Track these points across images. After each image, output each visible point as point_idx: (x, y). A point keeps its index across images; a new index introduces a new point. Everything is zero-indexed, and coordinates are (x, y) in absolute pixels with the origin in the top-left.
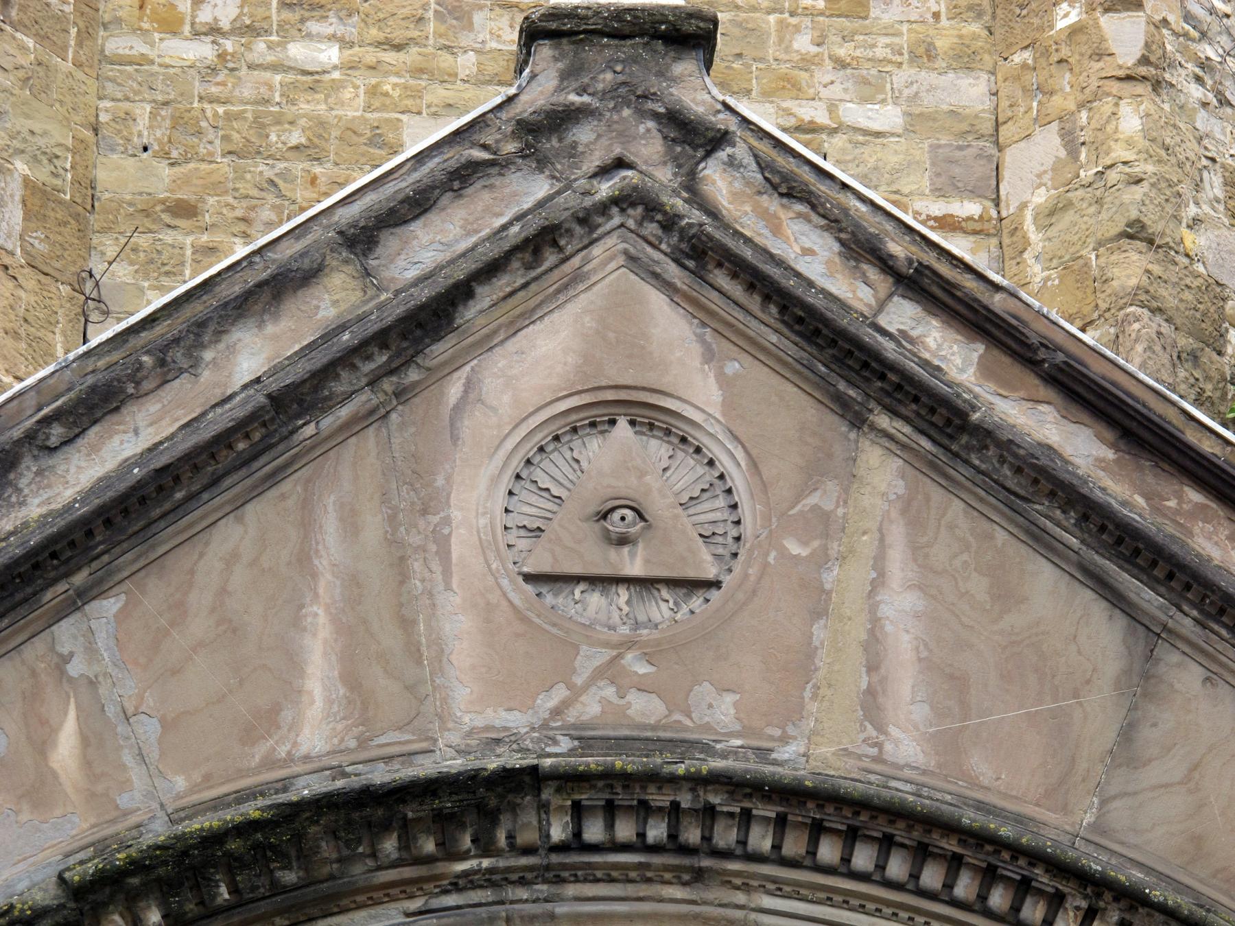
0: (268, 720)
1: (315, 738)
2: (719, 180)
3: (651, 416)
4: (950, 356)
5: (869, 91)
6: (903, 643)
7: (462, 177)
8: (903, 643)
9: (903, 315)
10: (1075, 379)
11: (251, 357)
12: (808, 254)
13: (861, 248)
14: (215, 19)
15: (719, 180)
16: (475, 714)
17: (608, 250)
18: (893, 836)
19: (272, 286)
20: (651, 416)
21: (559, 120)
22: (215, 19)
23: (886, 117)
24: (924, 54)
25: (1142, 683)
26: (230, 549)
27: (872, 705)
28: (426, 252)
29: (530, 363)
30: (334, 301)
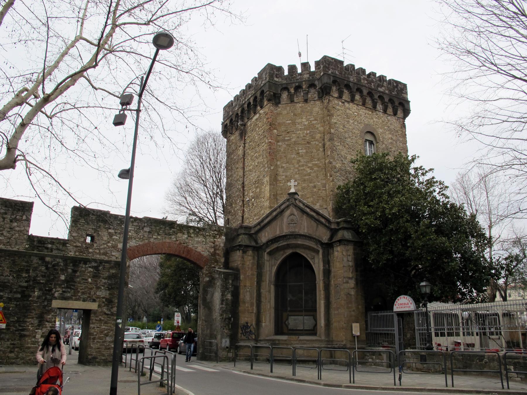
1: (278, 233)
2: (297, 202)
3: (294, 215)
4: (308, 210)
5: (319, 182)
9: (306, 208)
11: (274, 214)
13: (304, 204)
16: (286, 231)
17: (291, 207)
19: (275, 210)
20: (294, 215)
21: (289, 199)
23: (319, 184)
26: (274, 224)
27: (304, 229)
28: (283, 207)
29: (288, 213)
30: (278, 210)
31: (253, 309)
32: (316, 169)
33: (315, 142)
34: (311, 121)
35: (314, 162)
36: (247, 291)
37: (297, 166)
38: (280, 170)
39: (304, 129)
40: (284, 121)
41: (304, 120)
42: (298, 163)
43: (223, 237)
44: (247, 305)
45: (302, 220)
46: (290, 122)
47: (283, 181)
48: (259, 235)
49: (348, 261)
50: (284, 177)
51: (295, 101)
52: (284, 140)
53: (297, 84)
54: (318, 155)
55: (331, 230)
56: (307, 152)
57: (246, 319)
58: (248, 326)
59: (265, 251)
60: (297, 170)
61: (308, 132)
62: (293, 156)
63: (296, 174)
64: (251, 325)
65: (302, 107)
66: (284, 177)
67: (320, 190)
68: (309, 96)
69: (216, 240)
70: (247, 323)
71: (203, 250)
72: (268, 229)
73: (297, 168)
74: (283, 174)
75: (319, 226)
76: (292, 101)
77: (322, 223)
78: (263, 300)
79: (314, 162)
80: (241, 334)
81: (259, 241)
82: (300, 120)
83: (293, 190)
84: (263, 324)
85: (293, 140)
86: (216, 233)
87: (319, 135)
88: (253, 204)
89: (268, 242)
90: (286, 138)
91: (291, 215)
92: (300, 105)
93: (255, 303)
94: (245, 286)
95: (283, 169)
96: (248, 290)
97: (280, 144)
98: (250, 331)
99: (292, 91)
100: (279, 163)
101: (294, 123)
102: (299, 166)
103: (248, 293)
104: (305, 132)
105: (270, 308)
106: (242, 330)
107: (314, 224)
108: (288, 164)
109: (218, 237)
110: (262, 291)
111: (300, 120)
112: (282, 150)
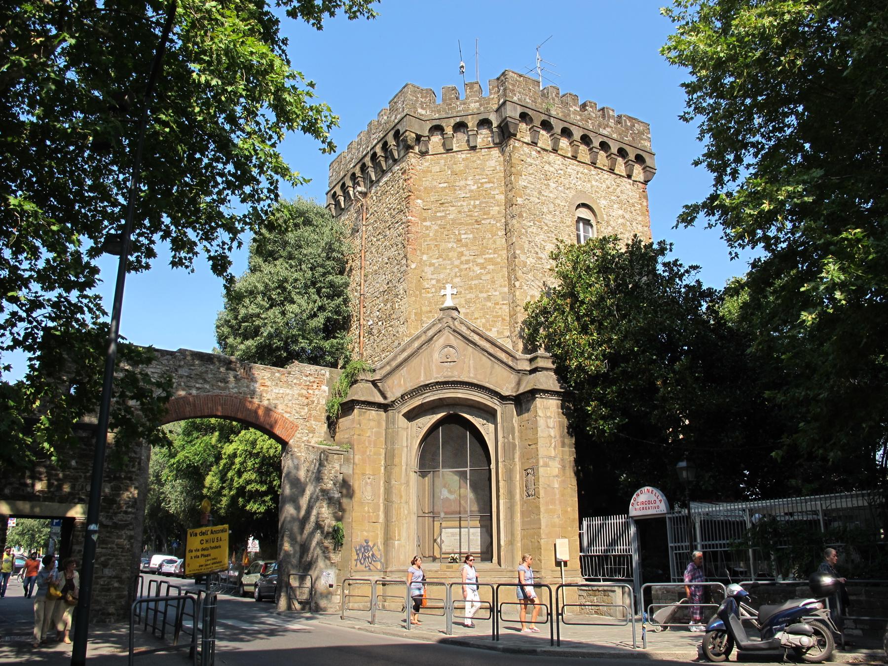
0: (418, 378)
1: (423, 380)
2: (456, 323)
3: (451, 346)
4: (476, 338)
5: (496, 291)
6: (472, 365)
7: (434, 325)
8: (472, 365)
9: (472, 334)
10: (576, 647)
11: (416, 344)
12: (464, 330)
13: (469, 328)
14: (698, 281)
15: (456, 323)
17: (446, 332)
18: (481, 269)
19: (418, 338)
21: (442, 318)
22: (698, 281)
23: (497, 293)
24: (501, 286)
25: (493, 367)
26: (415, 362)
27: (469, 372)
28: (430, 333)
29: (440, 341)
30: (423, 338)
31: (378, 515)
32: (491, 267)
33: (488, 221)
34: (482, 183)
35: (487, 256)
36: (367, 483)
37: (457, 262)
38: (428, 270)
39: (470, 198)
40: (435, 183)
41: (469, 182)
42: (459, 258)
43: (325, 388)
44: (366, 509)
45: (465, 355)
46: (445, 185)
47: (433, 290)
48: (390, 381)
49: (549, 427)
50: (434, 282)
51: (455, 149)
52: (434, 218)
53: (458, 120)
54: (495, 242)
55: (518, 371)
56: (475, 238)
57: (365, 533)
58: (368, 546)
59: (399, 412)
60: (457, 270)
61: (477, 202)
62: (450, 245)
63: (456, 276)
64: (374, 545)
65: (467, 159)
66: (434, 282)
67: (497, 304)
68: (479, 140)
69: (311, 392)
70: (367, 541)
71: (289, 410)
72: (404, 371)
73: (457, 267)
74: (433, 277)
75: (496, 366)
76: (449, 150)
77: (502, 362)
78: (395, 498)
79: (487, 256)
80: (356, 560)
81: (388, 395)
82: (462, 183)
83: (449, 303)
84: (396, 542)
85: (451, 217)
86: (311, 379)
87: (497, 208)
88: (379, 332)
89: (402, 396)
90: (439, 214)
91: (446, 346)
92: (463, 156)
93: (382, 505)
94: (364, 474)
95: (432, 268)
96: (369, 481)
97: (428, 223)
98: (373, 555)
99: (449, 131)
100: (425, 257)
101: (452, 188)
102: (462, 263)
103: (369, 488)
104: (472, 203)
105: (409, 513)
106: (358, 554)
107: (485, 360)
108: (441, 260)
109: (315, 385)
110: (393, 482)
111: (462, 183)
112: (431, 234)
